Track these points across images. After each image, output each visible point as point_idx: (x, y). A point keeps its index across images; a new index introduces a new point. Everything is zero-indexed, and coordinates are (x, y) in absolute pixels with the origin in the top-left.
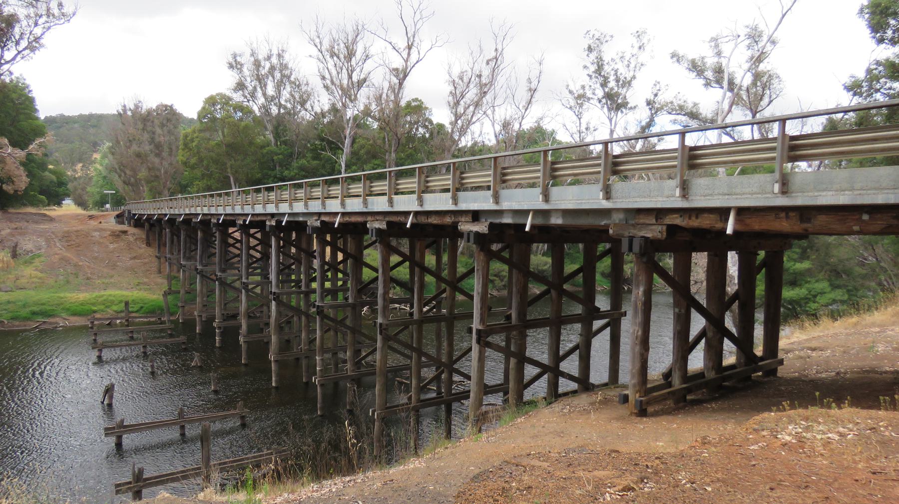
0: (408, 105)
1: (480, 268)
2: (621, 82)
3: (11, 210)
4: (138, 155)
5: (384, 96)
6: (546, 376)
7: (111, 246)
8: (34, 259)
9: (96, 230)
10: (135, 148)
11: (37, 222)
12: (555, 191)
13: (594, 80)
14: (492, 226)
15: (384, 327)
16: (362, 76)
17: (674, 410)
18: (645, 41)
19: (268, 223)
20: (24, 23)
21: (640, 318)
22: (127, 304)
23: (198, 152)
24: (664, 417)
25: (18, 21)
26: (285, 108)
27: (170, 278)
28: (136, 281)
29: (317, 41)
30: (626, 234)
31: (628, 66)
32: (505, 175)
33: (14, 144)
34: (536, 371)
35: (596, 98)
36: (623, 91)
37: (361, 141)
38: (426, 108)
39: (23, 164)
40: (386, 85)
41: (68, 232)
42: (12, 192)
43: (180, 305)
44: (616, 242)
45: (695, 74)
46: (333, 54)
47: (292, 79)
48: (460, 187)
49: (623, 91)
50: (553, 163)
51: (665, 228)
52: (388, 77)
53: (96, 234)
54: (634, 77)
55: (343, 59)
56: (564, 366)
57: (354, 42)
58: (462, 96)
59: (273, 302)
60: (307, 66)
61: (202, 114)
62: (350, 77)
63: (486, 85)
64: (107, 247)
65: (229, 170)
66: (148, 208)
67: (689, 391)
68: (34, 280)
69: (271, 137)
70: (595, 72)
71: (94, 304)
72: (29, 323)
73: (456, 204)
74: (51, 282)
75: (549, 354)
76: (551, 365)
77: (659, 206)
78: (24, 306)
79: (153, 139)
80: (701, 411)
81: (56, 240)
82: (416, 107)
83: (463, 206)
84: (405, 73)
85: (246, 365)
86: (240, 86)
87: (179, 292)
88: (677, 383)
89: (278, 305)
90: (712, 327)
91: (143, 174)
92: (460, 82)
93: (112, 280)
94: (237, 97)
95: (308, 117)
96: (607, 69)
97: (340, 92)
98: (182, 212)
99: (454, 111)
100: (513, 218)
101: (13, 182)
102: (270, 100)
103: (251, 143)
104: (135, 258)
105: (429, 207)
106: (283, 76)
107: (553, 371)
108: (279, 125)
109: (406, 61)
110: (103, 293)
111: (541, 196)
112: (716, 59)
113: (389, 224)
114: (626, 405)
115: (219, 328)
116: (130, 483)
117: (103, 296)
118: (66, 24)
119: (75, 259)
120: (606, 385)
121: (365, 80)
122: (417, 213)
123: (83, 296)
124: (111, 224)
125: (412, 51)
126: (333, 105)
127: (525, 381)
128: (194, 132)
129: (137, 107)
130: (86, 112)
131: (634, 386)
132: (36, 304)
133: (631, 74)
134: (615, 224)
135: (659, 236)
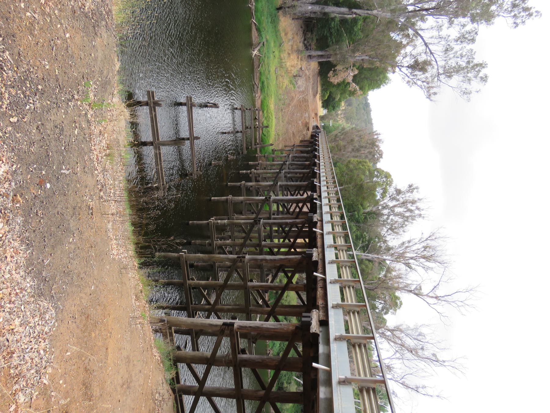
0: (397, 298)
1: (283, 326)
3: (319, 79)
5: (401, 281)
7: (300, 122)
9: (309, 115)
10: (356, 139)
11: (313, 88)
14: (316, 336)
15: (243, 259)
16: (413, 266)
19: (315, 194)
20: (423, 76)
22: (267, 127)
23: (356, 169)
25: (424, 74)
26: (388, 219)
27: (281, 151)
29: (433, 238)
33: (355, 77)
37: (370, 265)
40: (409, 282)
41: (308, 101)
42: (329, 75)
43: (266, 155)
47: (406, 223)
48: (348, 312)
50: (374, 390)
52: (415, 283)
53: (307, 115)
57: (435, 261)
59: (264, 198)
60: (413, 233)
61: (380, 171)
62: (412, 258)
64: (300, 120)
65: (346, 186)
66: (322, 140)
69: (368, 209)
71: (267, 112)
73: (333, 307)
78: (267, 78)
79: (362, 147)
82: (397, 303)
85: (227, 185)
86: (399, 192)
89: (263, 200)
91: (342, 143)
92: (417, 333)
93: (281, 122)
94: (391, 190)
95: (383, 233)
97: (401, 252)
98: (321, 171)
99: (396, 329)
100: (323, 353)
103: (364, 198)
104: (294, 134)
105: (330, 287)
106: (407, 217)
108: (376, 215)
109: (427, 295)
110: (274, 116)
111: (343, 377)
113: (316, 262)
115: (251, 173)
119: (292, 104)
121: (410, 268)
122: (324, 280)
123: (272, 106)
124: (313, 123)
125: (435, 299)
126: (392, 248)
127: (193, 365)
128: (368, 166)
129: (380, 141)
132: (268, 84)
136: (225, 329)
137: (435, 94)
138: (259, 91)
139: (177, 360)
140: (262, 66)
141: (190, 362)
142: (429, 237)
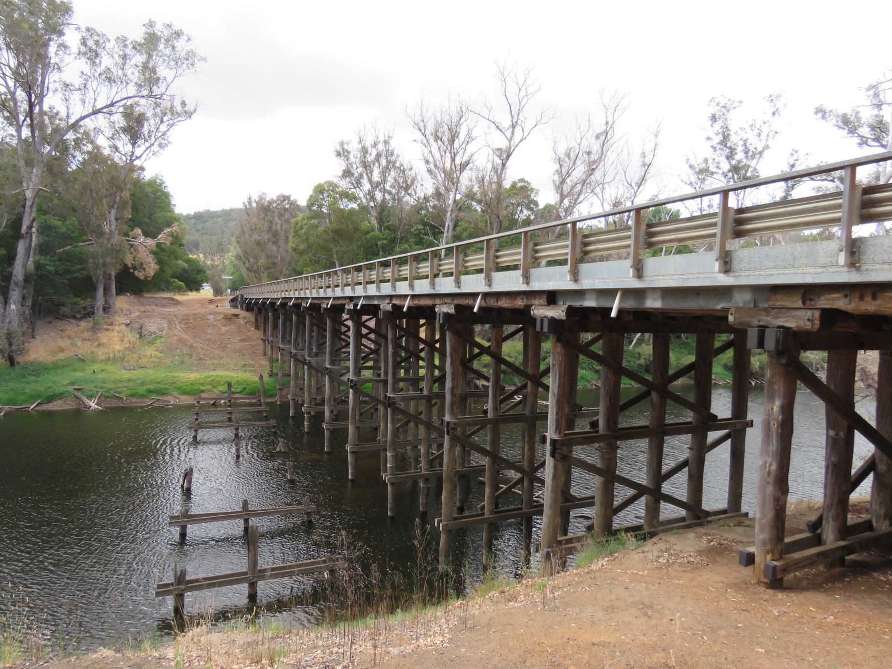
0: (514, 185)
1: (557, 363)
2: (751, 153)
4: (258, 244)
5: (487, 178)
6: (643, 499)
7: (224, 329)
8: (155, 340)
9: (211, 314)
10: (256, 236)
11: (164, 306)
12: (651, 264)
13: (718, 152)
14: (570, 311)
15: (452, 426)
16: (465, 158)
17: (827, 581)
18: (780, 104)
19: (347, 307)
20: (152, 122)
21: (774, 445)
22: (229, 385)
23: (307, 239)
24: (809, 595)
26: (390, 193)
27: (272, 361)
28: (243, 363)
29: (422, 124)
30: (755, 322)
31: (759, 135)
32: (586, 244)
33: (146, 234)
34: (630, 492)
35: (721, 172)
36: (753, 163)
37: (463, 224)
38: (532, 189)
39: (154, 253)
40: (490, 166)
41: (187, 315)
42: (142, 278)
44: (741, 333)
45: (846, 131)
46: (437, 138)
47: (398, 165)
49: (753, 163)
51: (817, 314)
53: (211, 317)
54: (767, 147)
55: (446, 143)
56: (667, 487)
57: (458, 124)
58: (569, 174)
59: (351, 390)
60: (412, 154)
61: (312, 202)
62: (453, 160)
63: (594, 162)
64: (220, 329)
65: (335, 256)
67: (849, 550)
68: (154, 359)
69: (374, 222)
70: (721, 143)
71: (202, 384)
72: (145, 400)
73: (528, 283)
74: (168, 361)
75: (648, 473)
76: (651, 486)
77: (809, 280)
78: (142, 384)
80: (872, 589)
81: (177, 322)
82: (522, 187)
83: (536, 286)
84: (508, 152)
85: (328, 453)
86: (347, 173)
87: (277, 375)
88: (830, 539)
89: (355, 393)
90: (885, 458)
91: (262, 261)
92: (566, 159)
93: (221, 362)
94: (344, 185)
96: (734, 139)
97: (443, 175)
98: (308, 295)
100: (597, 300)
101: (144, 269)
102: (375, 186)
103: (356, 229)
104: (243, 340)
105: (497, 287)
106: (388, 162)
107: (655, 494)
108: (383, 210)
109: (510, 140)
111: (631, 270)
112: (876, 112)
113: (457, 307)
114: (751, 568)
115: (309, 413)
116: (172, 584)
117: (210, 377)
118: (188, 120)
119: (191, 341)
120: (724, 512)
121: (468, 163)
122: (486, 295)
123: (194, 376)
124: (226, 307)
126: (437, 189)
128: (303, 219)
130: (228, 208)
131: (764, 543)
132: (152, 382)
133: (763, 143)
134: (737, 308)
135: (808, 326)
136: (560, 454)
137: (184, 104)
138: (165, 398)
139: (609, 531)
140: (119, 393)
141: (611, 511)
142: (420, 130)
